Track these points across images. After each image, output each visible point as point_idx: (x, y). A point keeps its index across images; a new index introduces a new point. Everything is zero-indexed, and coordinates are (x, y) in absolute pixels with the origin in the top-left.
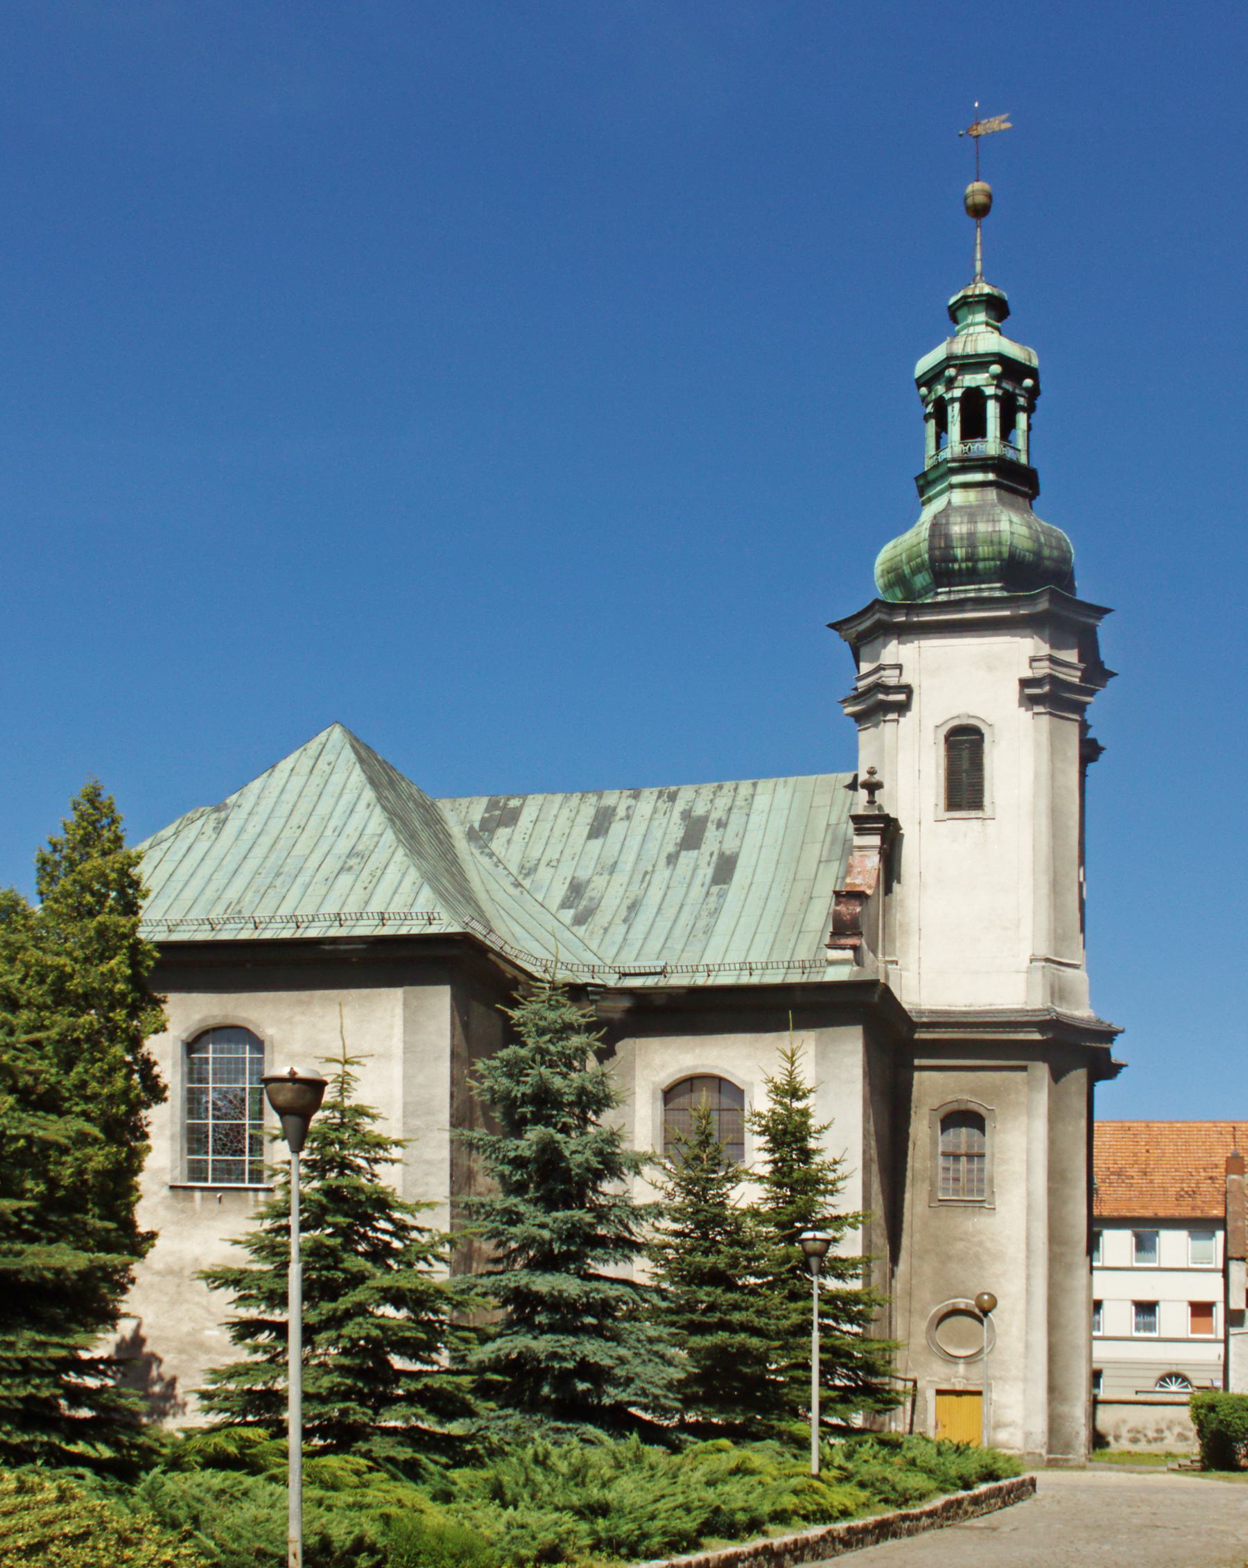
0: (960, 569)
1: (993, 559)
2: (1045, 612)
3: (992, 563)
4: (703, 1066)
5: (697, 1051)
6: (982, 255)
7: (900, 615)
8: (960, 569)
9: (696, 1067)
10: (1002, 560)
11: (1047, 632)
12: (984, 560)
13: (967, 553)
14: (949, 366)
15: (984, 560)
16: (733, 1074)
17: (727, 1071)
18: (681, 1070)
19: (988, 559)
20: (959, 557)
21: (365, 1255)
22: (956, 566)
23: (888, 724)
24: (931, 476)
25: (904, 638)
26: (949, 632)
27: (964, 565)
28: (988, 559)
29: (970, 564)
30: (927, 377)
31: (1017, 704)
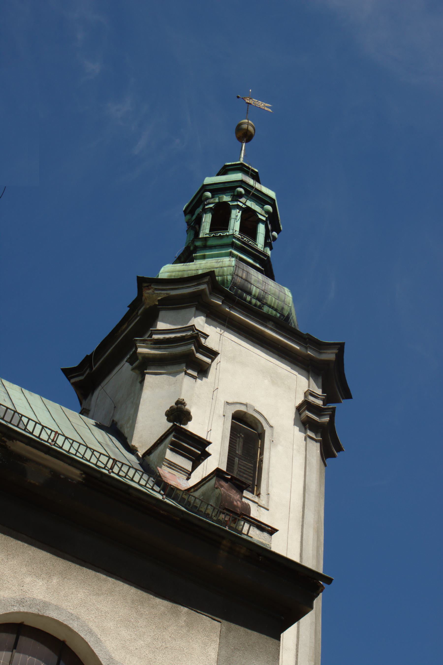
0: (250, 302)
1: (276, 310)
2: (327, 363)
3: (274, 312)
4: (57, 608)
5: (55, 580)
6: (244, 156)
7: (219, 299)
8: (250, 302)
9: (46, 605)
10: (282, 315)
11: (320, 381)
12: (270, 306)
13: (259, 294)
14: (241, 187)
15: (270, 306)
16: (98, 641)
17: (91, 632)
18: (21, 602)
19: (273, 308)
20: (253, 293)
21: (267, 212)
22: (248, 298)
23: (187, 377)
24: (209, 243)
25: (210, 320)
26: (246, 337)
27: (254, 301)
28: (273, 308)
29: (259, 303)
30: (215, 187)
31: (292, 422)
